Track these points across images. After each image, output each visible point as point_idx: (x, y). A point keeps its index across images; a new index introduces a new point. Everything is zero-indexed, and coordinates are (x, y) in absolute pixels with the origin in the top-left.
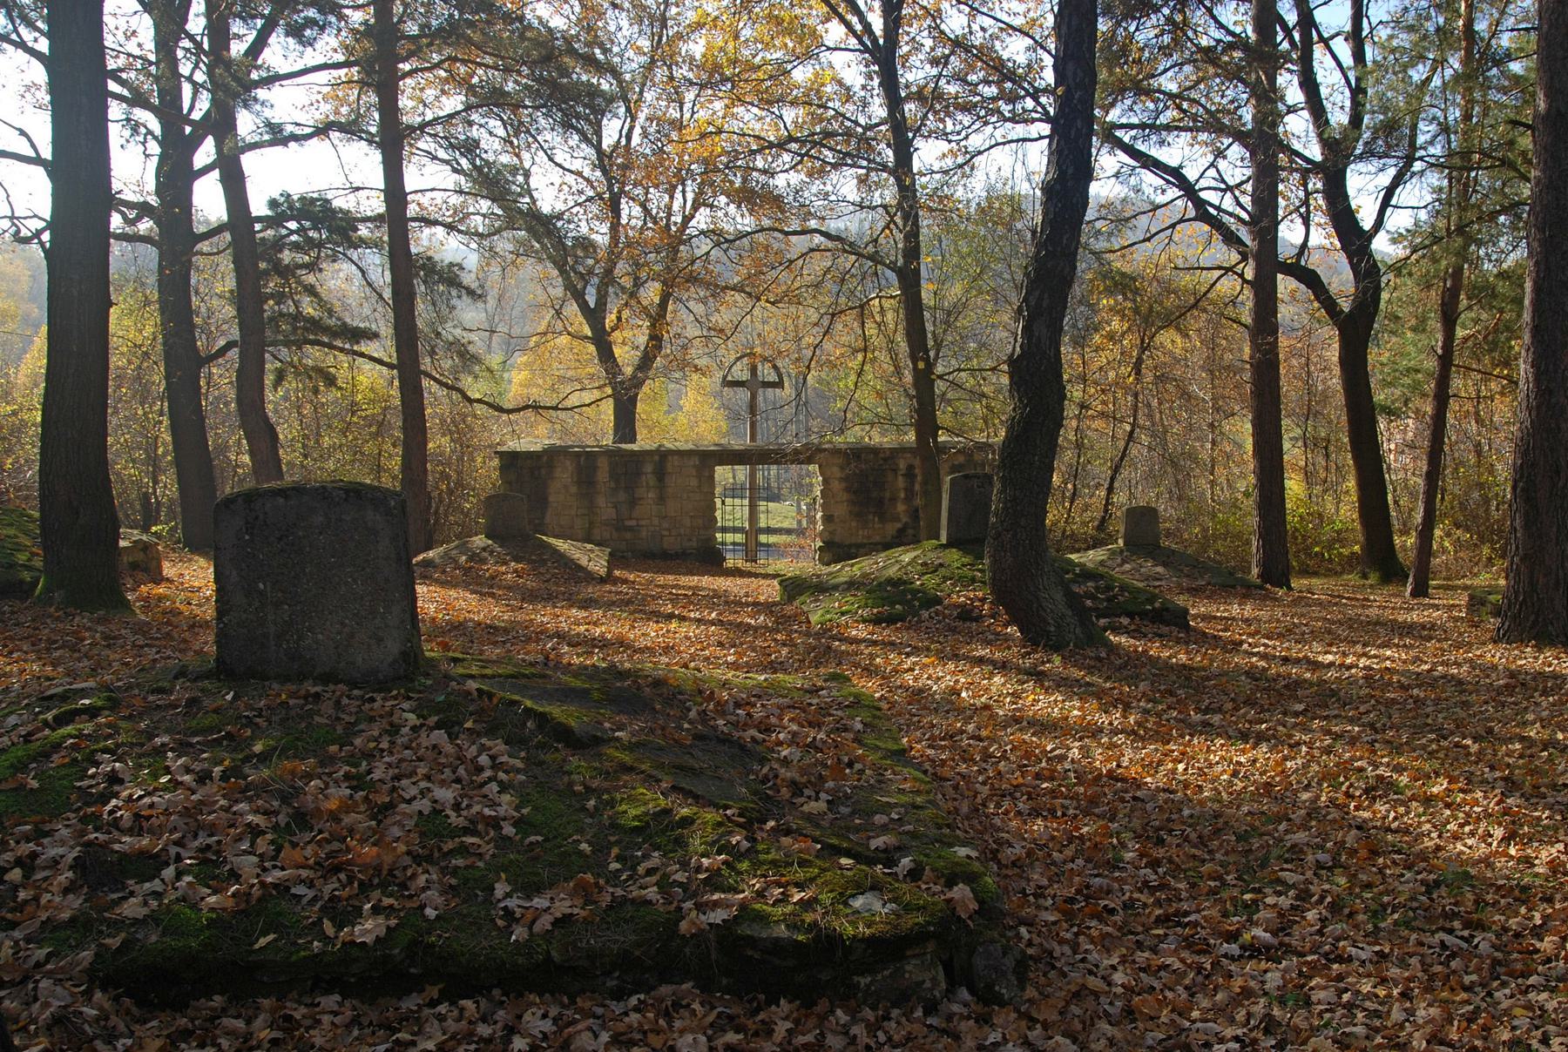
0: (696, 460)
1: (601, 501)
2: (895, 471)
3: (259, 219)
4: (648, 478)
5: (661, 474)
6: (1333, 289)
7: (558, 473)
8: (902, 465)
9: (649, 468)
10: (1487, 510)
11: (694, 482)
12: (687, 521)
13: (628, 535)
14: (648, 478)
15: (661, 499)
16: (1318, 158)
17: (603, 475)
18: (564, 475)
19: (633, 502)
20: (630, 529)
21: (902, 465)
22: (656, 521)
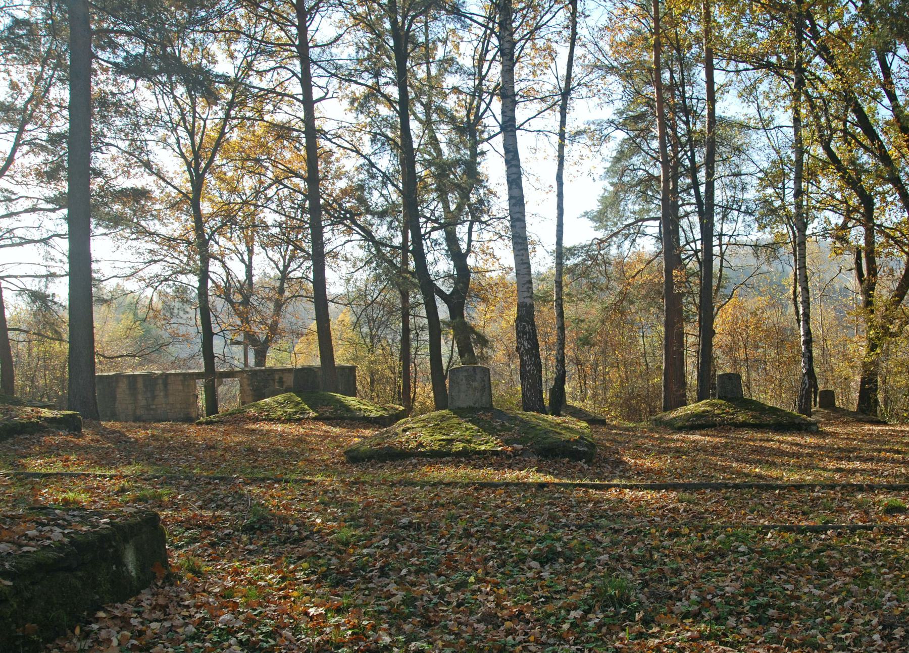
0: (181, 378)
1: (140, 397)
2: (274, 380)
3: (444, 322)
4: (160, 386)
5: (166, 384)
6: (254, 272)
7: (121, 384)
8: (277, 377)
9: (160, 381)
10: (420, 257)
11: (181, 388)
12: (178, 406)
13: (152, 412)
14: (160, 386)
15: (166, 396)
16: (303, 117)
17: (140, 385)
18: (140, 380)
19: (154, 397)
20: (152, 409)
21: (277, 377)
22: (164, 405)
